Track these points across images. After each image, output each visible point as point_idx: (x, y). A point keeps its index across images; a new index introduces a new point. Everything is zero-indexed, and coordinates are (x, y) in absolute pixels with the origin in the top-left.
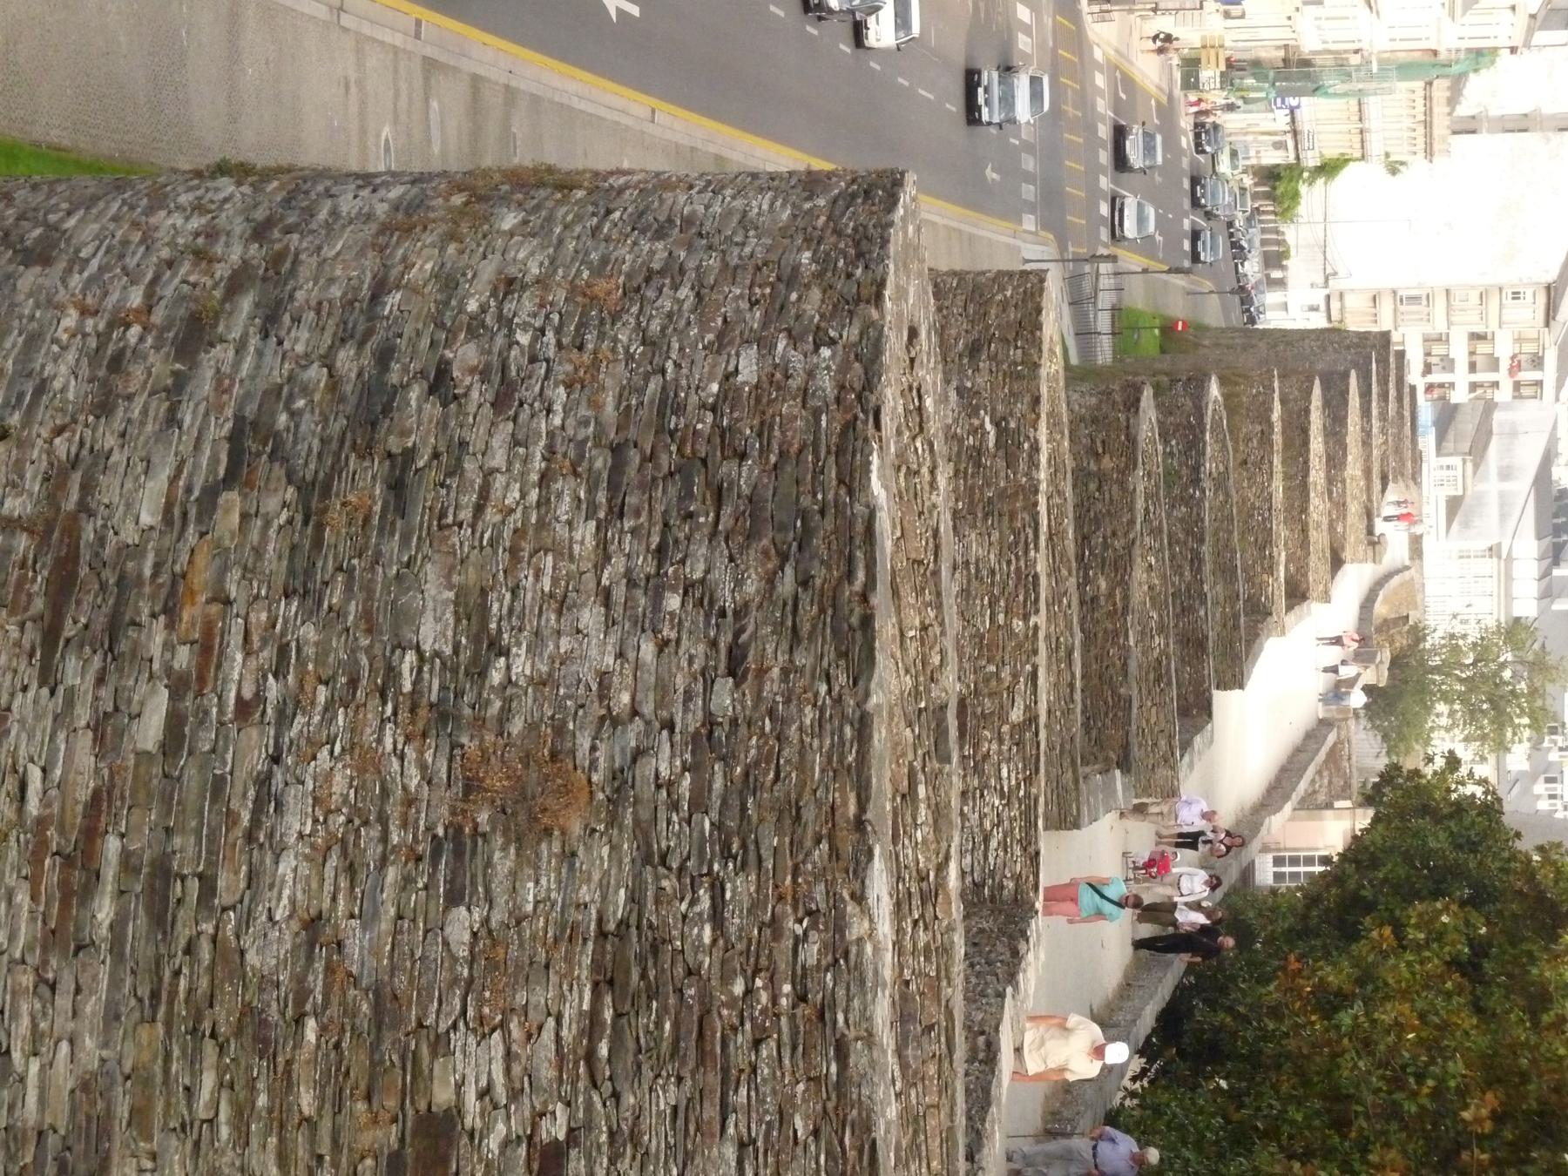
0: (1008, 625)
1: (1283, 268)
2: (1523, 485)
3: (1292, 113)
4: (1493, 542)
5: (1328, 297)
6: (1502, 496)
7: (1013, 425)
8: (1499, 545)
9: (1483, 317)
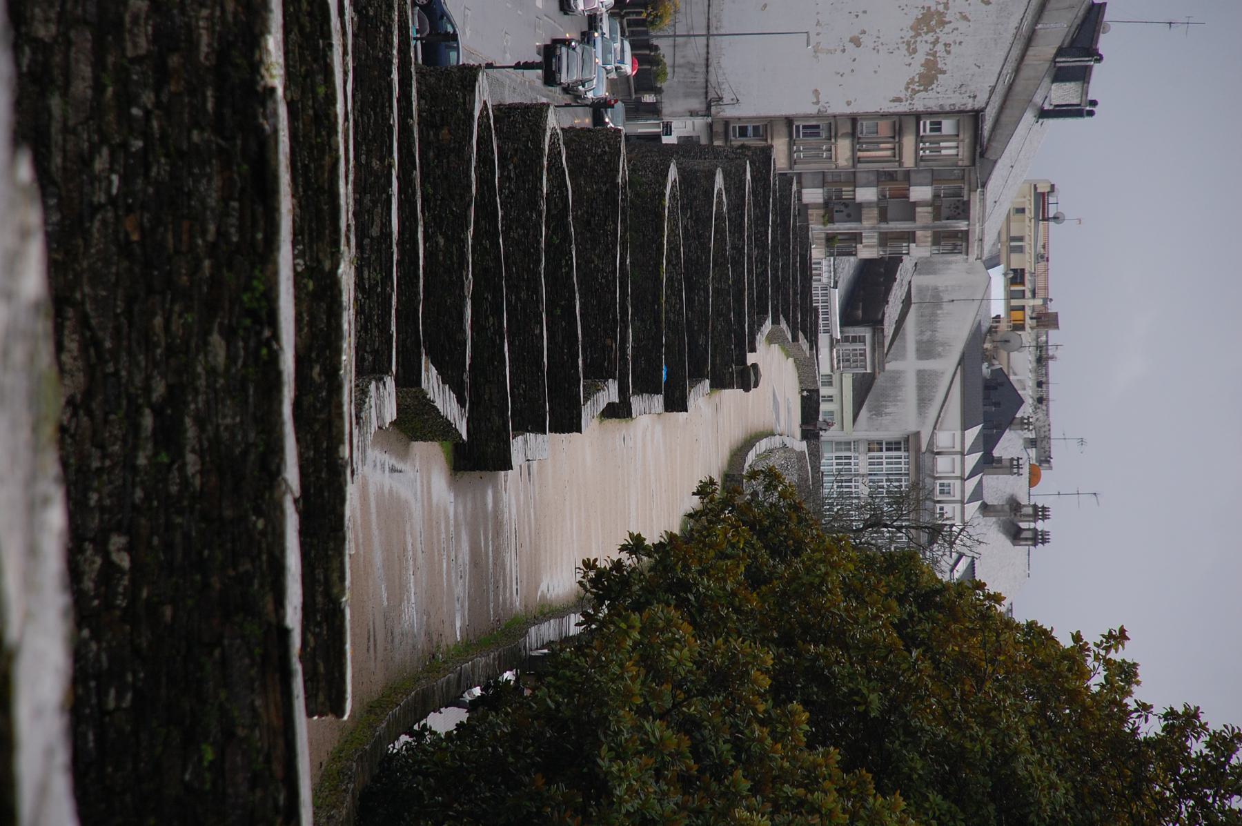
0: (368, 164)
1: (658, 91)
2: (946, 365)
4: (912, 428)
5: (710, 126)
6: (921, 375)
7: (371, 13)
8: (917, 434)
9: (898, 153)
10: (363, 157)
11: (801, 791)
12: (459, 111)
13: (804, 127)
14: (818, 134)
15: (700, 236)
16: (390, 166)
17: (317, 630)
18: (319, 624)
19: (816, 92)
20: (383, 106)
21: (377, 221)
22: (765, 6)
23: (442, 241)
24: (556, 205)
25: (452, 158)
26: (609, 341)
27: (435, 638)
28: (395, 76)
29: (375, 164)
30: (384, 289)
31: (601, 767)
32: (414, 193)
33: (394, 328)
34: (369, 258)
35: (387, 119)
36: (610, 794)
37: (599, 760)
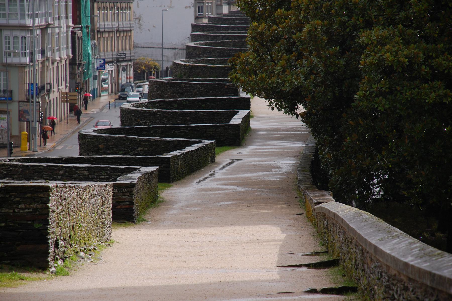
0: (61, 175)
3: (108, 62)
7: (5, 172)
10: (59, 177)
11: (302, 12)
12: (93, 141)
13: (199, 12)
14: (202, 7)
15: (210, 52)
16: (62, 167)
17: (13, 197)
18: (11, 196)
19: (186, 7)
20: (40, 169)
21: (83, 172)
22: (154, 26)
23: (140, 149)
24: (162, 105)
25: (109, 144)
26: (226, 87)
27: (298, 154)
28: (29, 164)
29: (61, 172)
30: (109, 170)
31: (290, 90)
32: (93, 158)
33: (124, 167)
34: (97, 176)
35: (44, 168)
36: (298, 87)
37: (287, 91)
